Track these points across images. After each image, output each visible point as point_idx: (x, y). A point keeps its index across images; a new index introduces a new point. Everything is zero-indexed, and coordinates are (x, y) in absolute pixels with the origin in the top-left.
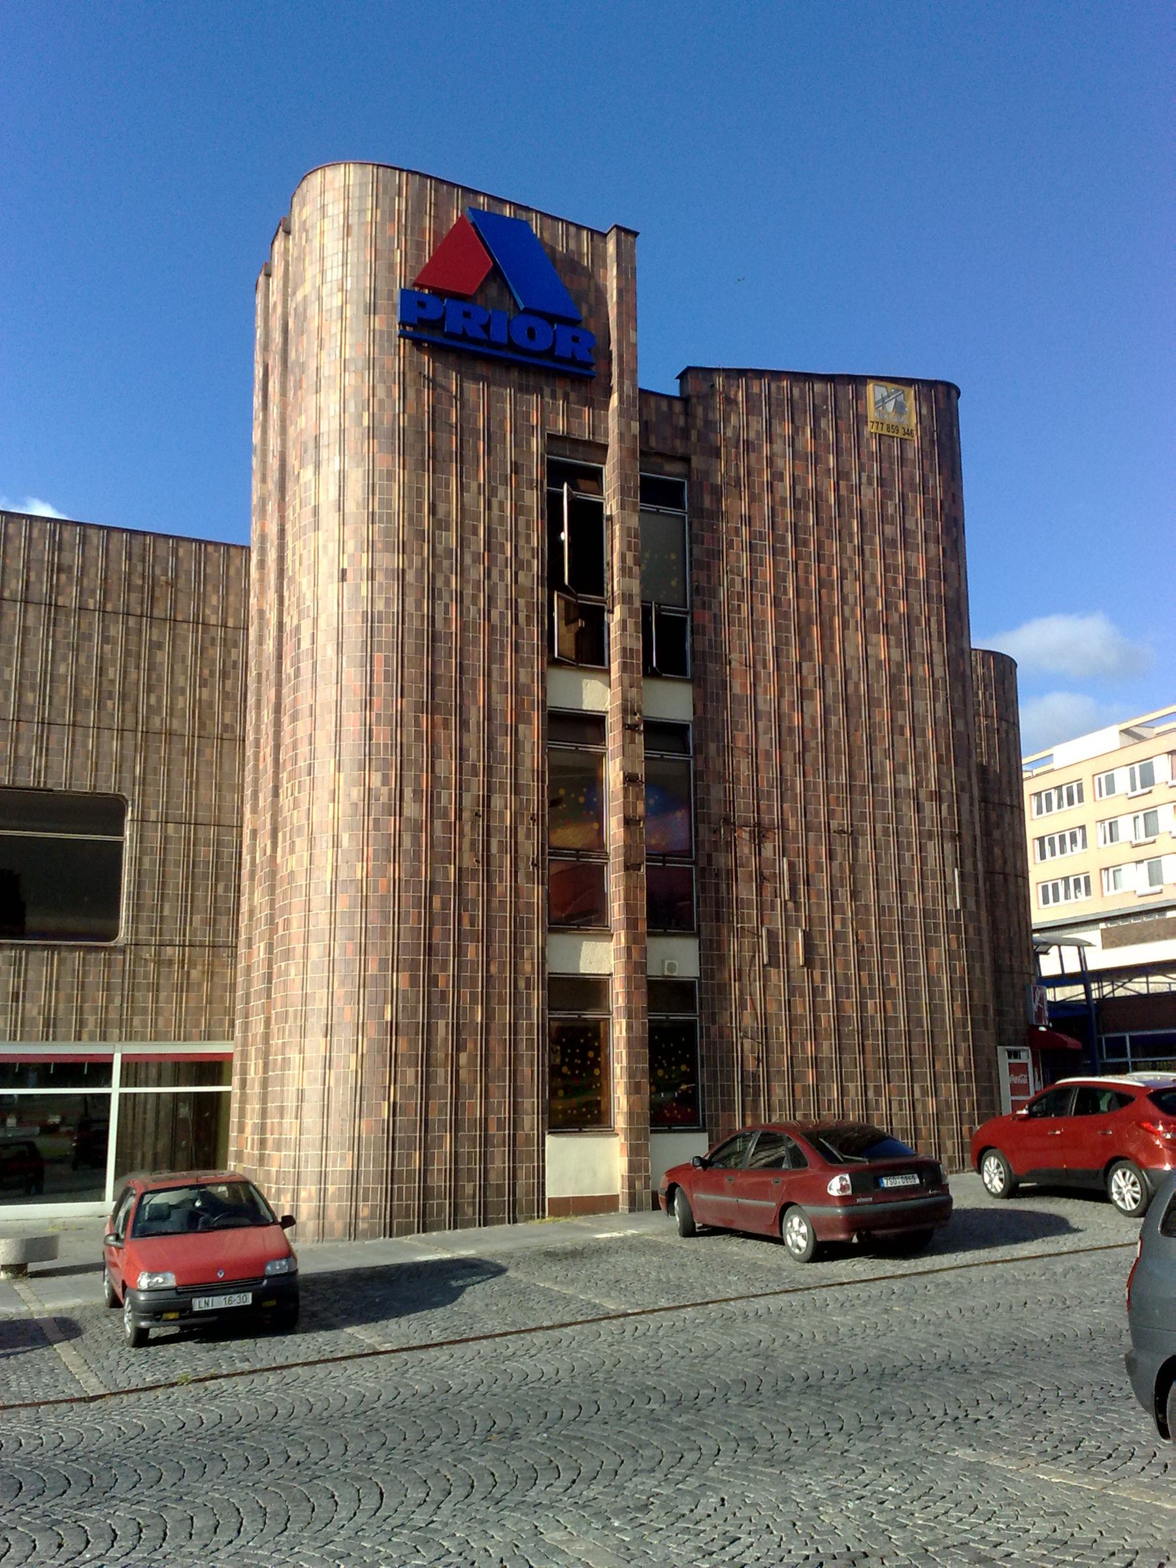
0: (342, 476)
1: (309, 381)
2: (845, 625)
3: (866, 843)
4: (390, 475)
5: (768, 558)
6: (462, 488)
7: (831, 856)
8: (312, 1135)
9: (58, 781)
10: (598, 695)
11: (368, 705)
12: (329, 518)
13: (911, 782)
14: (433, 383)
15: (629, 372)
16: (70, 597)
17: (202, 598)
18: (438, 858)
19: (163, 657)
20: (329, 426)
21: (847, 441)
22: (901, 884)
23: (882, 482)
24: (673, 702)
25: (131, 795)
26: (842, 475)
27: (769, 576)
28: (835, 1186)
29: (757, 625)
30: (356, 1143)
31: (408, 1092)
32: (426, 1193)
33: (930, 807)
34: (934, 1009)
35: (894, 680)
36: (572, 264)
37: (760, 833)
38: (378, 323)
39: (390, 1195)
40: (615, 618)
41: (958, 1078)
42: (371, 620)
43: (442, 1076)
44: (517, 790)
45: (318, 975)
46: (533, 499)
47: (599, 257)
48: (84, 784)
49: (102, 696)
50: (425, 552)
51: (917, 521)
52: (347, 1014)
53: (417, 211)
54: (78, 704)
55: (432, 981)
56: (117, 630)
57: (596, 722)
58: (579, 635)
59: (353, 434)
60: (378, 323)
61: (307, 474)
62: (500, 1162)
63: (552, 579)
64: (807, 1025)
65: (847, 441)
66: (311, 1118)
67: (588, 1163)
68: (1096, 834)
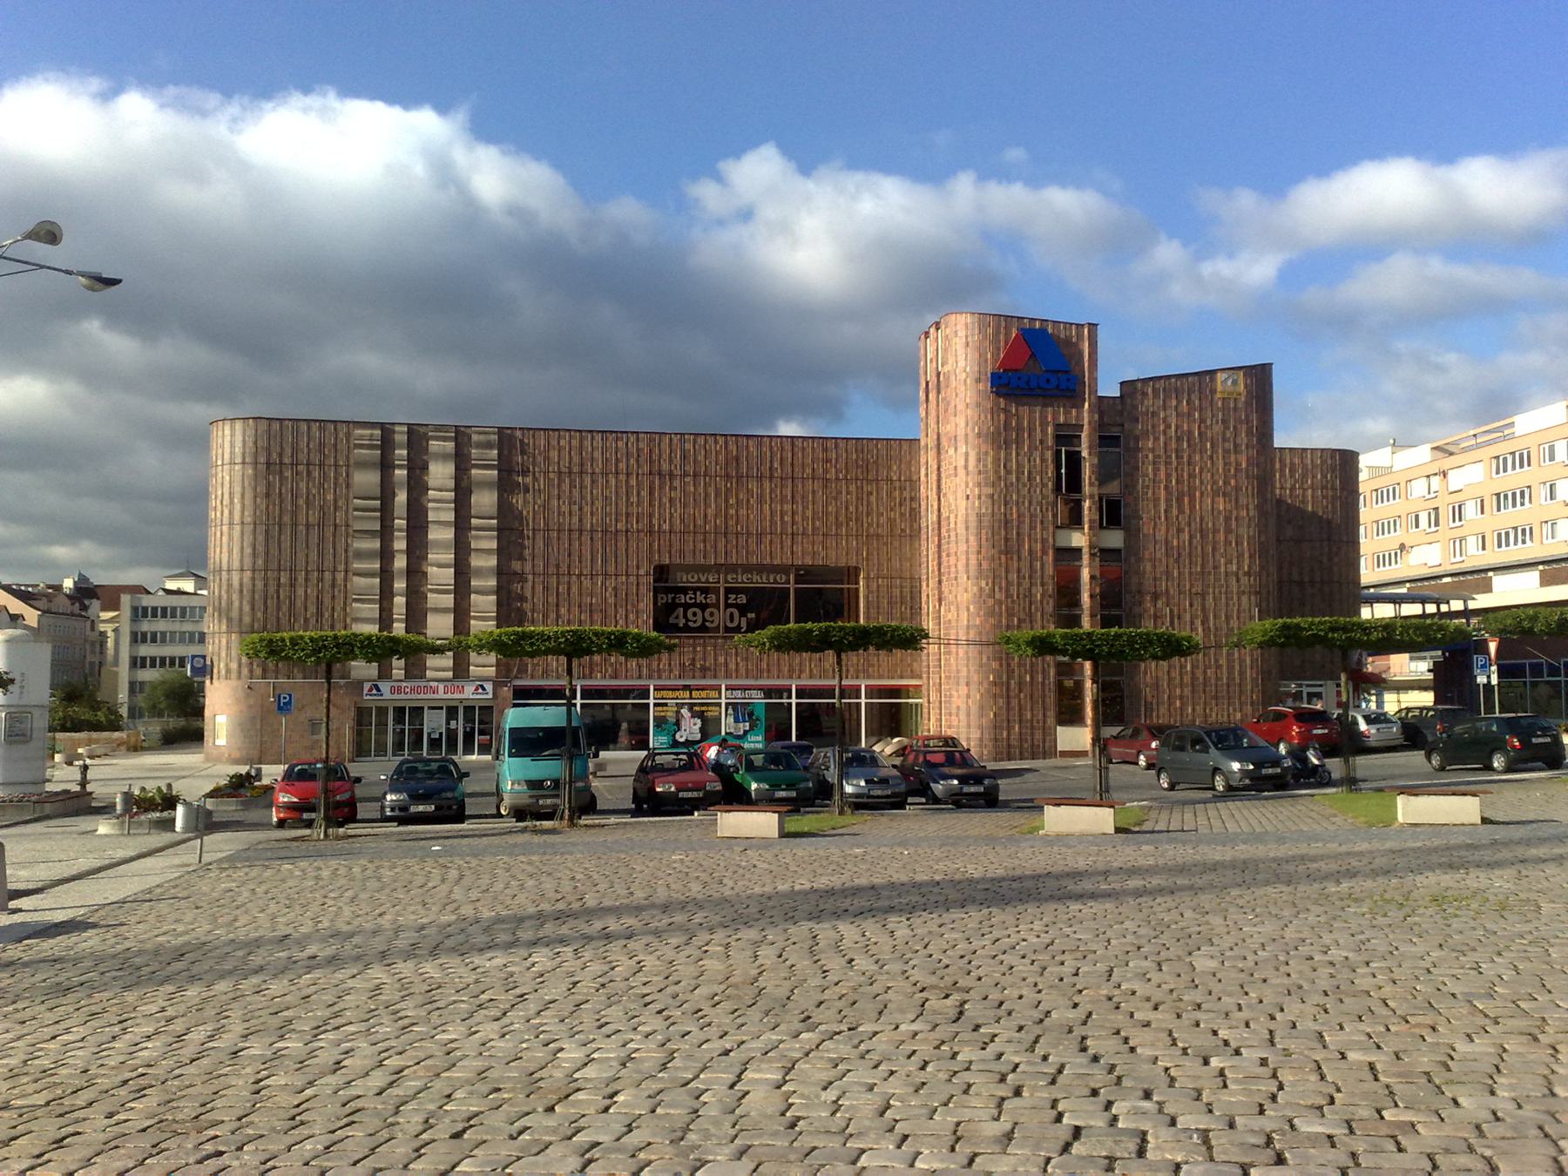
0: (967, 454)
1: (951, 409)
2: (1202, 494)
3: (1210, 598)
4: (986, 453)
5: (1163, 468)
6: (1018, 454)
7: (1191, 605)
8: (964, 723)
9: (832, 562)
10: (1079, 539)
11: (979, 552)
12: (961, 472)
13: (1234, 568)
14: (1005, 411)
15: (1094, 390)
16: (832, 475)
17: (890, 468)
18: (1010, 615)
19: (873, 498)
20: (961, 432)
21: (1206, 404)
22: (1227, 617)
23: (1224, 421)
24: (1115, 539)
25: (863, 565)
26: (1202, 421)
27: (1163, 476)
28: (1154, 745)
29: (1156, 500)
30: (981, 727)
31: (1000, 708)
32: (1009, 746)
33: (1244, 580)
34: (1242, 673)
35: (1228, 519)
36: (1068, 342)
37: (1156, 597)
38: (981, 386)
39: (995, 747)
40: (1087, 504)
41: (1252, 704)
42: (979, 516)
43: (1014, 702)
44: (1043, 584)
45: (962, 662)
46: (1049, 455)
47: (1080, 336)
48: (842, 563)
49: (848, 520)
50: (1003, 488)
51: (1243, 438)
52: (975, 678)
53: (997, 333)
54: (838, 525)
55: (1008, 665)
56: (853, 488)
57: (1079, 550)
58: (1071, 510)
59: (971, 436)
60: (981, 386)
61: (951, 451)
62: (1038, 735)
63: (1057, 488)
64: (1177, 681)
65: (1206, 404)
66: (963, 716)
67: (1078, 737)
68: (1541, 493)
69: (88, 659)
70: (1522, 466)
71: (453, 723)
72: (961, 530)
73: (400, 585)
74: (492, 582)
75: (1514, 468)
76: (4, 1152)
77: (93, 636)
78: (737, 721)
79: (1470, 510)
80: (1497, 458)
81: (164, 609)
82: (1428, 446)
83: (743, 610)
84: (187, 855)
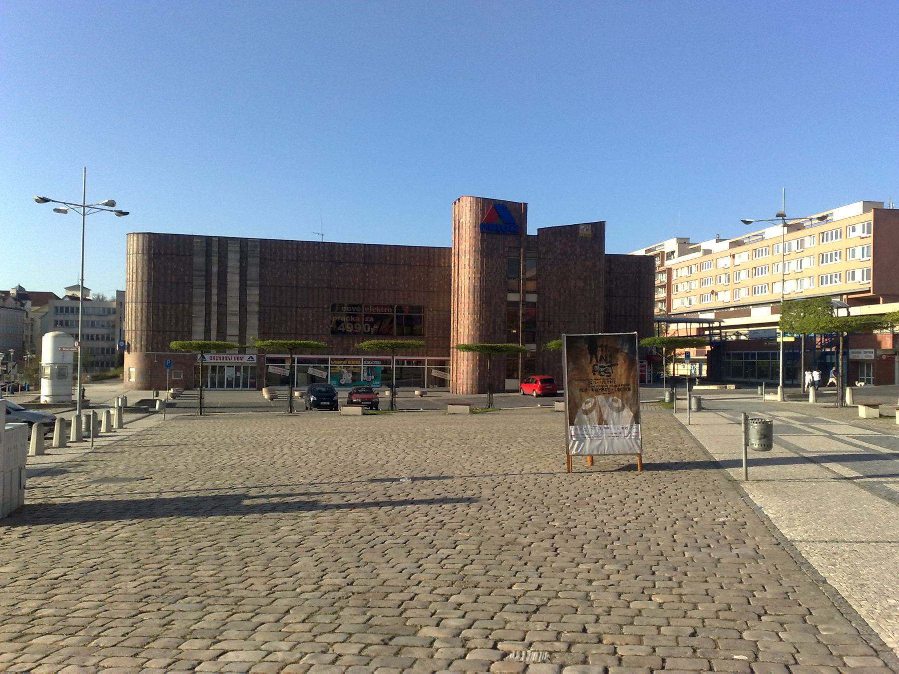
12: (467, 267)
42: (475, 287)
69: (25, 333)
70: (836, 238)
71: (238, 374)
72: (467, 293)
73: (214, 309)
74: (257, 309)
75: (832, 239)
76: (1, 590)
77: (28, 321)
78: (368, 375)
79: (743, 274)
80: (823, 233)
81: (67, 308)
82: (727, 242)
83: (372, 325)
84: (160, 417)
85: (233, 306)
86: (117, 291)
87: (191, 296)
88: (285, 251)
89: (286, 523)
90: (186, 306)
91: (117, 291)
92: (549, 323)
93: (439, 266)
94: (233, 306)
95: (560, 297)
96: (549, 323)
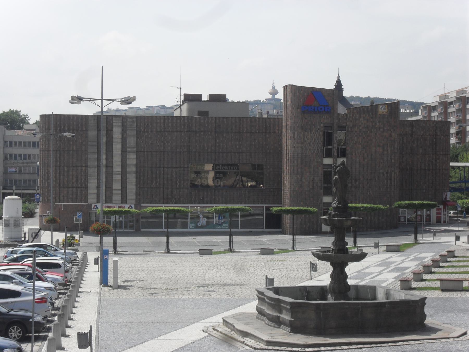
60: (299, 110)
71: (121, 218)
73: (103, 170)
74: (134, 169)
78: (219, 219)
85: (117, 168)
86: (40, 115)
87: (87, 159)
88: (155, 124)
89: (232, 288)
90: (84, 168)
91: (40, 115)
92: (356, 181)
93: (274, 132)
94: (117, 168)
95: (364, 160)
96: (356, 181)
